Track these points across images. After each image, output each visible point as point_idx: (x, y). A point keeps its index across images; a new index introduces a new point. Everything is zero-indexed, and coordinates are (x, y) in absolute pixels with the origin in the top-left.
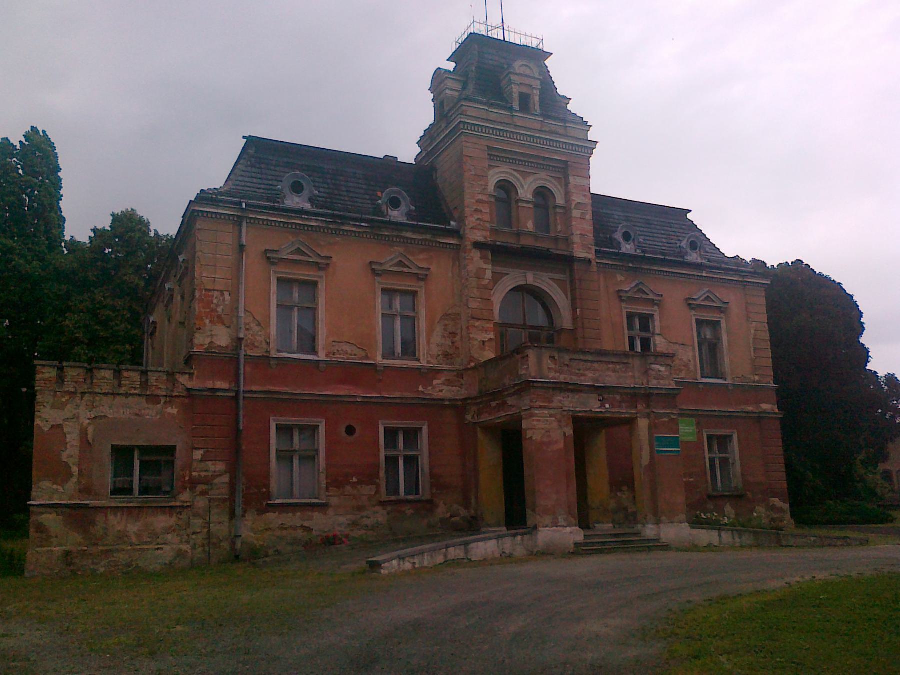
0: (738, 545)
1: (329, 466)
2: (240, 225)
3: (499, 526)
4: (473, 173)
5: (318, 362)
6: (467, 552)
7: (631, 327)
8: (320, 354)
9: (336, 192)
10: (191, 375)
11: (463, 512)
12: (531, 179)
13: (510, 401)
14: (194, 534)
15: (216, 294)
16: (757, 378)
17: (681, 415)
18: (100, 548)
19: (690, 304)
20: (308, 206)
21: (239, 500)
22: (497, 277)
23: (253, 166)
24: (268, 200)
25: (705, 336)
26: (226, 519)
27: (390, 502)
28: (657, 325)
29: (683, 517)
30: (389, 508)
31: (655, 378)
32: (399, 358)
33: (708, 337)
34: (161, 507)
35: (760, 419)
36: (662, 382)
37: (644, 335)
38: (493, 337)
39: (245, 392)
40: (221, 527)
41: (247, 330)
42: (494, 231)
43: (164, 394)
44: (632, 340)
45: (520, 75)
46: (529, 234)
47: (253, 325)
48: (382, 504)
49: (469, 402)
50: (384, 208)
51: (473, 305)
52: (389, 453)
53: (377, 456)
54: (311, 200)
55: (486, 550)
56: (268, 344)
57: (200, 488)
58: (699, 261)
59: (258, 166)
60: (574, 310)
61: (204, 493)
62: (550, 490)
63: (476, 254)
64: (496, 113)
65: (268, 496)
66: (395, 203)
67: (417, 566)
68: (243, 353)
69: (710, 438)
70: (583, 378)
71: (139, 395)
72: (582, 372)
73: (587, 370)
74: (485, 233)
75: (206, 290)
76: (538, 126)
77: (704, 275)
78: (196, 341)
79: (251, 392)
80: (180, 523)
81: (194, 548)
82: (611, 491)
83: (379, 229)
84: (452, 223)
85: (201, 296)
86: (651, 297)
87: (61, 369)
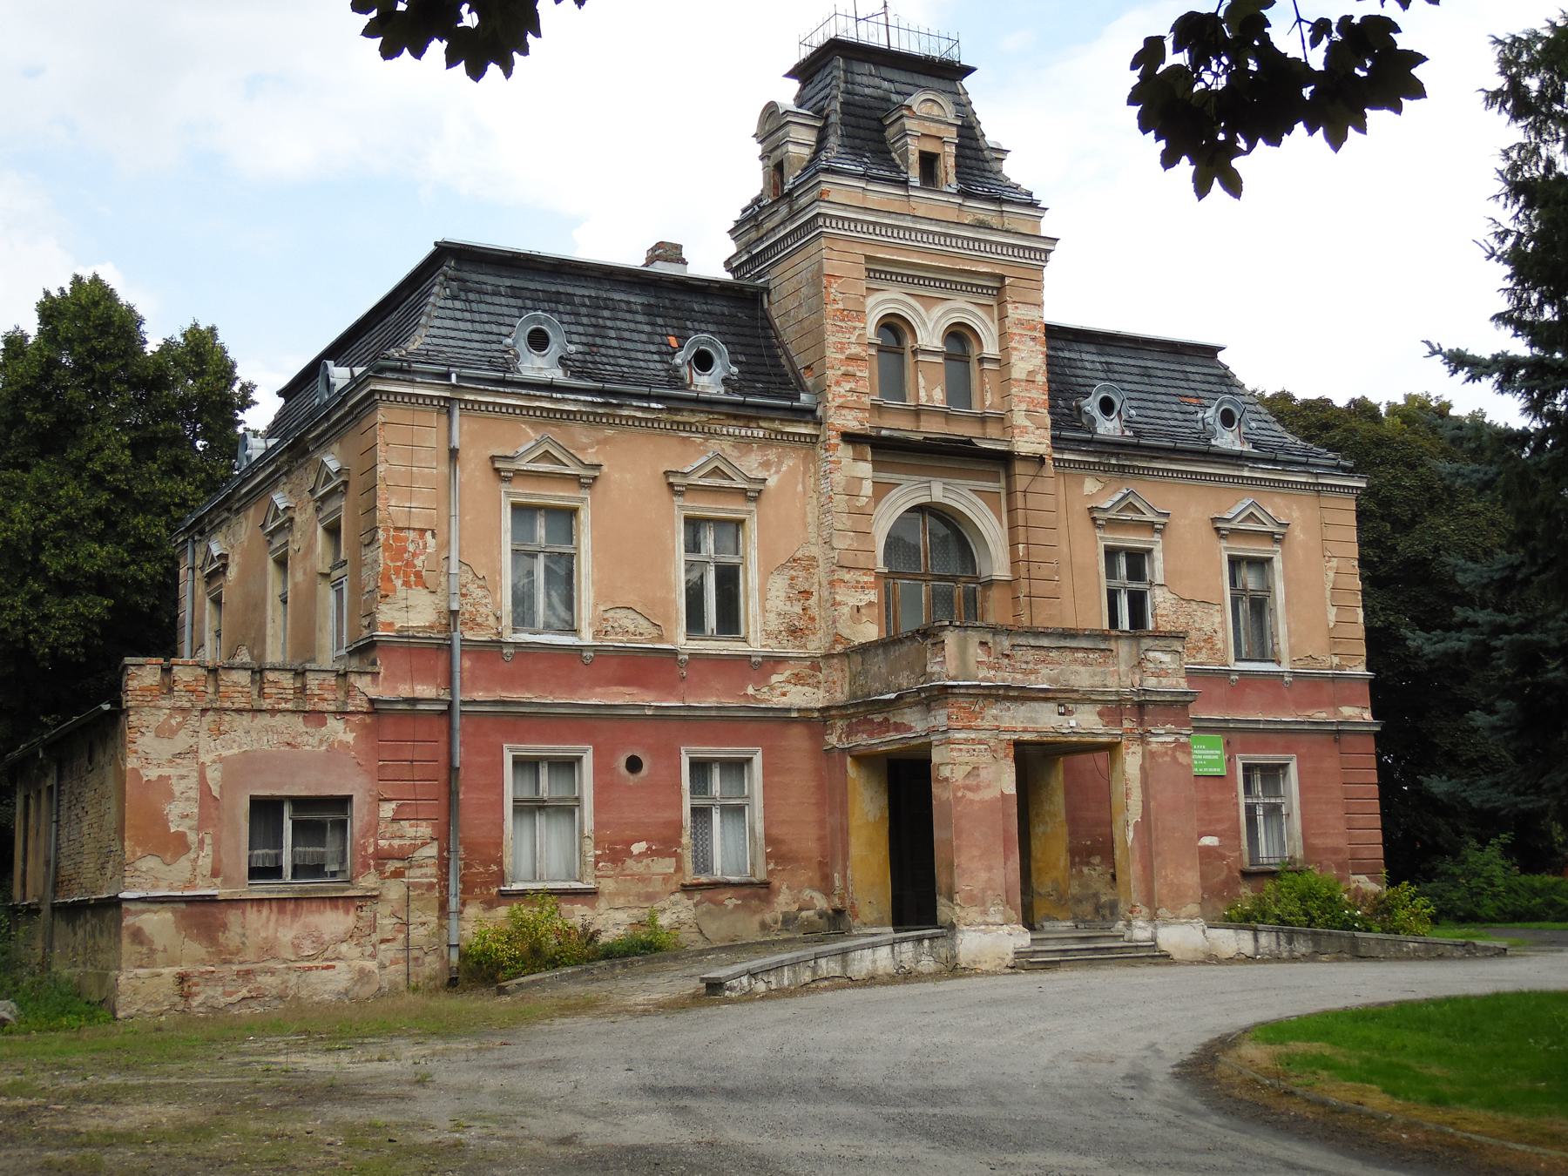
0: (1285, 955)
1: (598, 825)
2: (449, 413)
3: (882, 925)
4: (841, 306)
5: (580, 649)
6: (845, 967)
7: (1111, 572)
8: (583, 635)
9: (598, 341)
10: (375, 675)
11: (821, 902)
12: (938, 310)
14: (383, 941)
15: (412, 535)
16: (1336, 660)
18: (235, 968)
20: (558, 375)
21: (454, 886)
22: (881, 489)
23: (454, 298)
25: (1245, 585)
26: (432, 918)
27: (698, 887)
28: (1157, 568)
29: (1193, 908)
30: (697, 897)
32: (711, 638)
33: (1251, 586)
34: (331, 898)
35: (1338, 734)
36: (1164, 681)
37: (1135, 585)
38: (874, 598)
39: (463, 703)
41: (463, 595)
42: (877, 408)
43: (332, 708)
44: (1112, 595)
46: (934, 412)
47: (472, 587)
48: (687, 889)
49: (833, 712)
50: (685, 370)
51: (841, 543)
52: (697, 802)
54: (563, 361)
55: (874, 962)
56: (498, 619)
57: (391, 866)
58: (1238, 447)
60: (1013, 545)
61: (398, 874)
62: (977, 864)
63: (845, 452)
64: (881, 195)
65: (501, 877)
66: (703, 362)
67: (773, 987)
68: (457, 637)
69: (1248, 769)
70: (1033, 677)
71: (293, 712)
72: (1031, 666)
75: (397, 529)
77: (1246, 474)
78: (381, 618)
79: (474, 702)
80: (360, 925)
81: (383, 967)
82: (1073, 864)
84: (803, 396)
85: (387, 539)
86: (1150, 517)
87: (167, 671)
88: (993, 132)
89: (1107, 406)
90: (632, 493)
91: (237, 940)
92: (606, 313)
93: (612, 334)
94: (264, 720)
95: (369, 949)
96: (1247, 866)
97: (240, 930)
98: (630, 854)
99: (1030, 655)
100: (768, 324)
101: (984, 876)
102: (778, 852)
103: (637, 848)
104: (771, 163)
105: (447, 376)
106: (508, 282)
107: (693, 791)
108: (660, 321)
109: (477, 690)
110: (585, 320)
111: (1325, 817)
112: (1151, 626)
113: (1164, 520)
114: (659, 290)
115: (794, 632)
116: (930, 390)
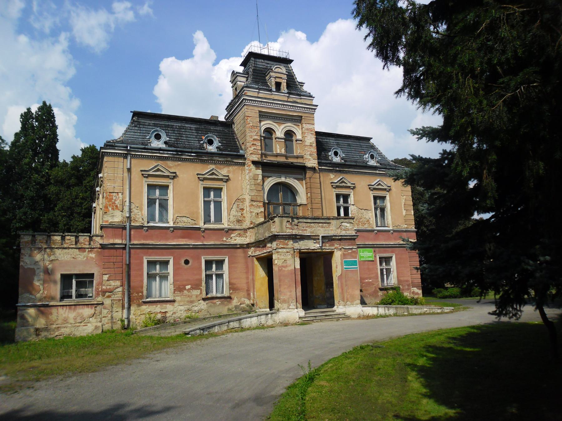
3: (266, 308)
4: (251, 125)
9: (180, 138)
12: (283, 126)
13: (269, 245)
16: (406, 226)
17: (358, 247)
19: (372, 188)
20: (164, 146)
23: (135, 126)
24: (142, 144)
28: (351, 200)
31: (344, 230)
32: (213, 224)
36: (348, 232)
37: (345, 205)
39: (207, 220)
40: (120, 314)
43: (88, 247)
44: (338, 209)
45: (275, 72)
46: (281, 155)
48: (204, 299)
53: (201, 275)
54: (166, 143)
55: (251, 322)
57: (107, 294)
59: (138, 126)
63: (253, 167)
64: (263, 94)
65: (142, 297)
66: (211, 142)
69: (380, 258)
73: (307, 227)
74: (258, 156)
76: (286, 99)
79: (134, 244)
82: (327, 288)
83: (202, 156)
88: (299, 78)
89: (336, 154)
90: (186, 181)
91: (56, 318)
92: (183, 130)
93: (184, 136)
94: (66, 251)
95: (99, 320)
96: (380, 286)
97: (56, 315)
98: (185, 289)
99: (304, 225)
100: (233, 133)
101: (288, 294)
102: (232, 287)
103: (188, 287)
104: (234, 88)
105: (127, 147)
106: (153, 122)
107: (206, 269)
108: (200, 132)
109: (136, 240)
110: (176, 132)
111: (403, 271)
112: (350, 215)
113: (353, 186)
114: (213, 123)
115: (239, 221)
116: (279, 148)
